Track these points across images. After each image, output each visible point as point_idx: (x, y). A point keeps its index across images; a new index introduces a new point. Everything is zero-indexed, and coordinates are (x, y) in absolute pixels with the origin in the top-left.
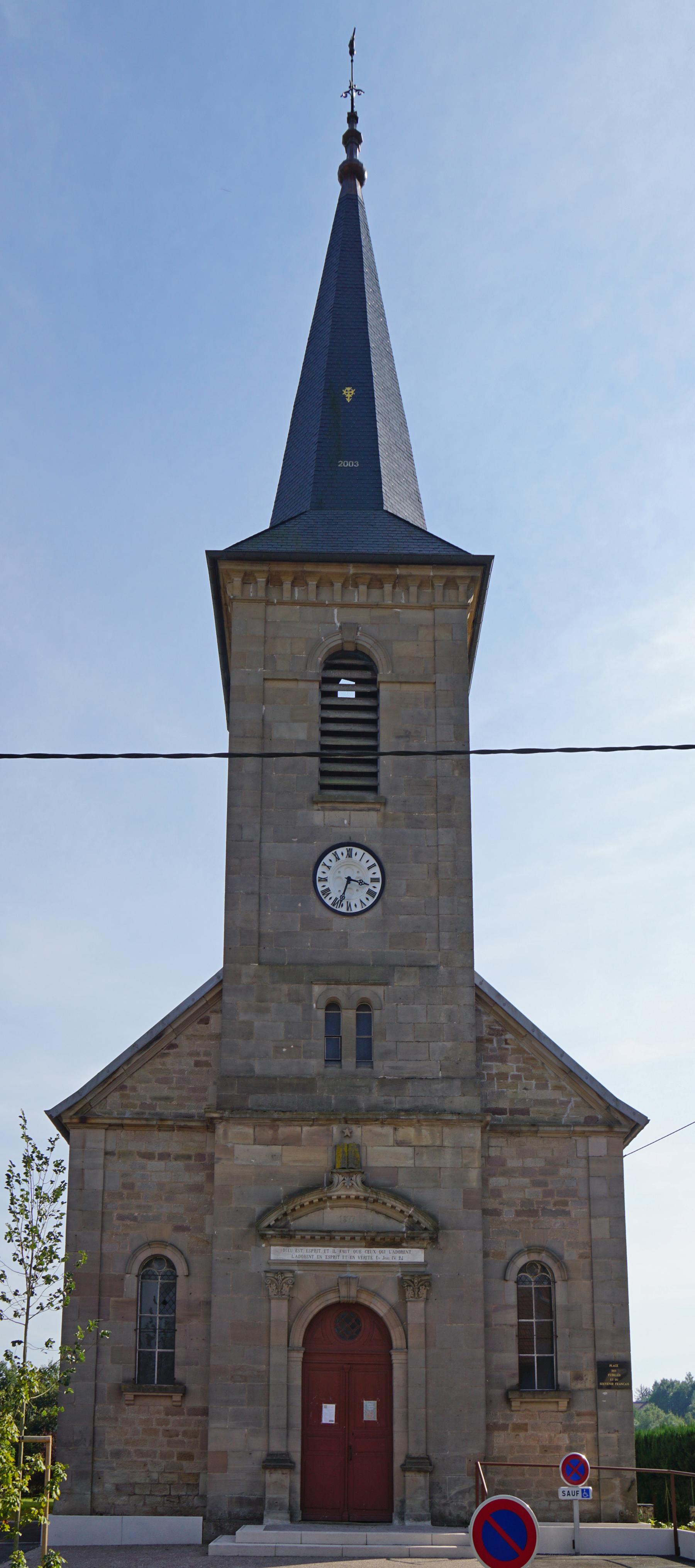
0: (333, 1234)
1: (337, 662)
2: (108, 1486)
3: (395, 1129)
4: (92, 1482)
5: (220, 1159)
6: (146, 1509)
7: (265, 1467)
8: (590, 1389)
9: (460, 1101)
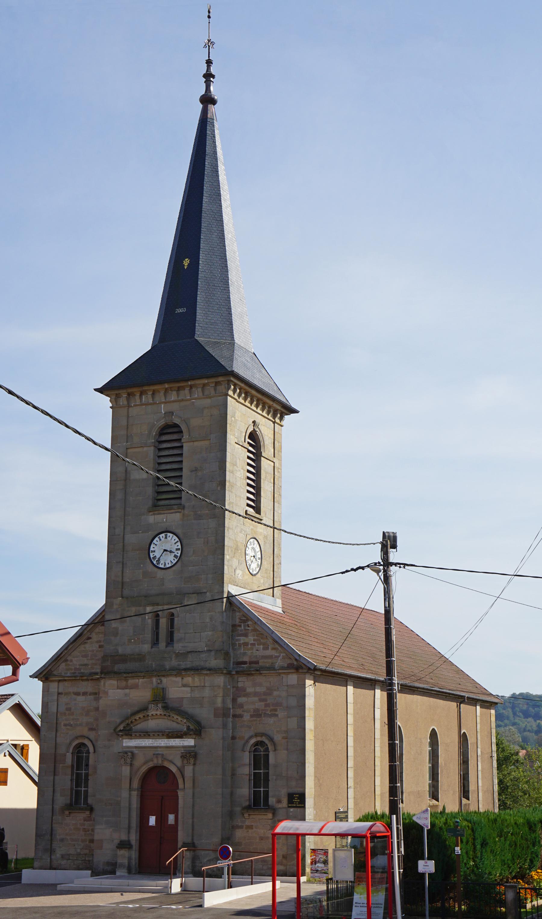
0: (149, 733)
1: (165, 432)
2: (58, 855)
3: (182, 678)
4: (51, 853)
5: (101, 697)
6: (75, 866)
7: (117, 847)
8: (285, 808)
9: (215, 662)
